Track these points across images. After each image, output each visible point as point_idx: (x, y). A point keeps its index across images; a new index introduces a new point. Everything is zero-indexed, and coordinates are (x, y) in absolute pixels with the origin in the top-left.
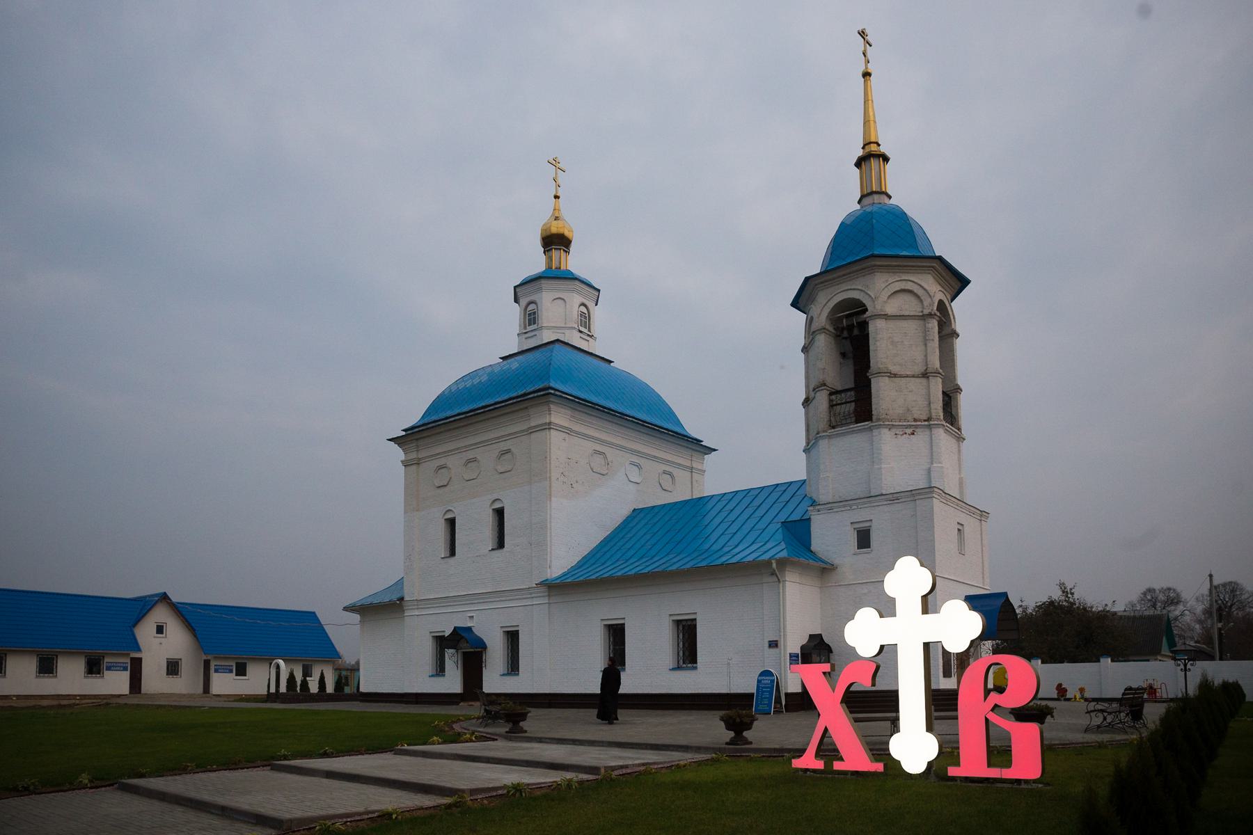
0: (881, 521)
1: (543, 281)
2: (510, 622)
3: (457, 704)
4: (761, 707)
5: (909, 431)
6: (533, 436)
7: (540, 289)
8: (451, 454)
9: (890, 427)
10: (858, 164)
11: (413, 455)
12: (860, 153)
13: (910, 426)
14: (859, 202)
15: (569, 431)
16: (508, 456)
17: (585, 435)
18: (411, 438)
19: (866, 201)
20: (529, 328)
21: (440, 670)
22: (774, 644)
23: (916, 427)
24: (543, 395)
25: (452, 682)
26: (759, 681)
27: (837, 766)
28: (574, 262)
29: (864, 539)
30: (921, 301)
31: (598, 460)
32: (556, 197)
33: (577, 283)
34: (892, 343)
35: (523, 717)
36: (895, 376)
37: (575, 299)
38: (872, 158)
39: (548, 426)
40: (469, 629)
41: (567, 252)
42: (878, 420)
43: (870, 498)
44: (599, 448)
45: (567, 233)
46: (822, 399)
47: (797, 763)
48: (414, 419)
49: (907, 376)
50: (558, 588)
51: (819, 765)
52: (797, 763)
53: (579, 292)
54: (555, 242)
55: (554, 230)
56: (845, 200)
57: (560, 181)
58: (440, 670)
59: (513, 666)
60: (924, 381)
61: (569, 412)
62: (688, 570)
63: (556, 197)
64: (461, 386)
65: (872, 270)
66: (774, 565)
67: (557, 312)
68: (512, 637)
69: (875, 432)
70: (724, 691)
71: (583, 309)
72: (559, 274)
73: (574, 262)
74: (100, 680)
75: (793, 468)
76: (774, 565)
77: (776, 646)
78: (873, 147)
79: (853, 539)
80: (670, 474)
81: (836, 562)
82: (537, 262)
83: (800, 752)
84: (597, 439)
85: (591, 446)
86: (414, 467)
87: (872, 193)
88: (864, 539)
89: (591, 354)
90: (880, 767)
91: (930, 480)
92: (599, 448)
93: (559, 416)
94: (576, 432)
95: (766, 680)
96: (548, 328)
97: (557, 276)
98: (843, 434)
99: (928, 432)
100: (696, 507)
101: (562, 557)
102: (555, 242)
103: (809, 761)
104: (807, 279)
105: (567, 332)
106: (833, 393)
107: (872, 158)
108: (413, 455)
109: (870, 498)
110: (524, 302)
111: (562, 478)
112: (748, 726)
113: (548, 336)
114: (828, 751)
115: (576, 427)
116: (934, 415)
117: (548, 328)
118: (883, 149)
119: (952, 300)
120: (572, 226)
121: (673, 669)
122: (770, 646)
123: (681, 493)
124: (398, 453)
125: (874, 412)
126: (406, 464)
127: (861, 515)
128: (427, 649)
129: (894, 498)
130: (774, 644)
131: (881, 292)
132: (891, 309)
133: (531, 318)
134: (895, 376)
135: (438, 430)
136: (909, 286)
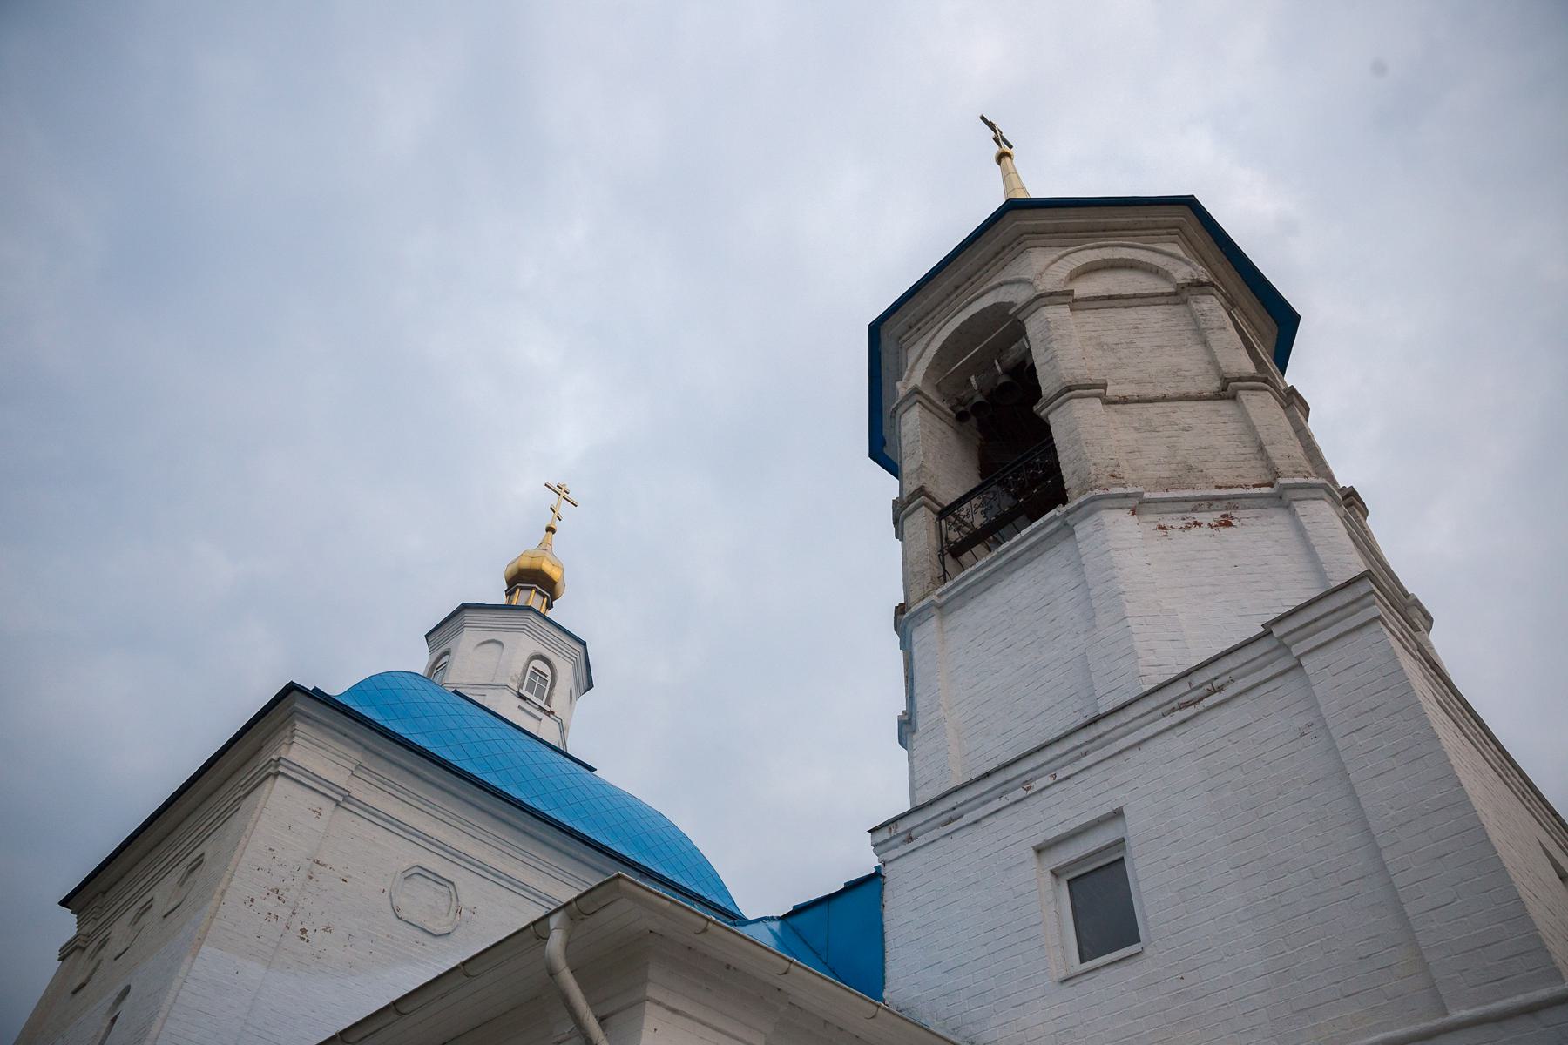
13: (1211, 501)
32: (550, 530)
34: (1100, 345)
46: (922, 522)
49: (1164, 399)
53: (532, 633)
60: (1225, 407)
61: (357, 756)
69: (1083, 529)
79: (1053, 914)
85: (410, 854)
89: (541, 741)
99: (1280, 517)
104: (875, 329)
106: (944, 513)
111: (271, 904)
116: (1282, 465)
119: (1282, 365)
120: (562, 562)
125: (1066, 471)
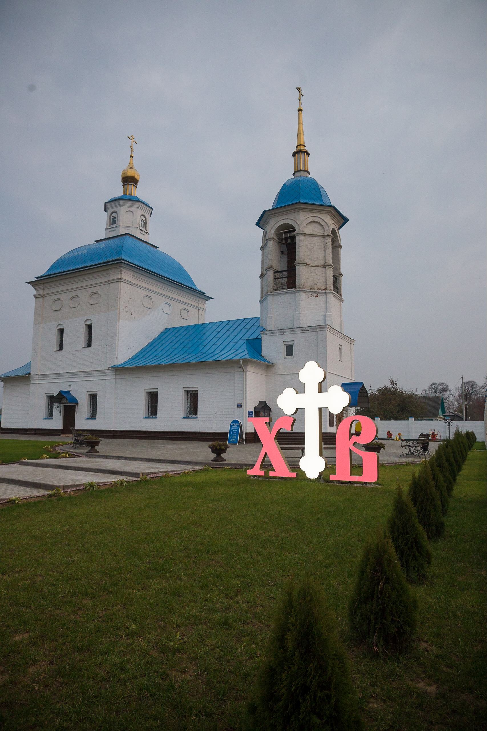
0: (299, 341)
1: (121, 201)
2: (93, 389)
3: (59, 435)
4: (231, 440)
5: (315, 295)
6: (111, 285)
7: (119, 205)
8: (82, 289)
9: (305, 292)
10: (294, 155)
11: (41, 292)
12: (295, 149)
14: (293, 175)
15: (132, 284)
16: (77, 299)
17: (140, 286)
18: (40, 282)
19: (298, 174)
20: (112, 226)
21: (50, 415)
22: (240, 406)
23: (319, 293)
24: (118, 263)
25: (57, 422)
26: (231, 426)
27: (271, 474)
28: (140, 192)
29: (290, 350)
30: (323, 228)
31: (146, 301)
32: (131, 157)
33: (140, 203)
35: (97, 443)
36: (309, 265)
37: (138, 212)
38: (300, 153)
39: (120, 280)
40: (68, 392)
41: (136, 187)
42: (299, 288)
43: (294, 329)
44: (147, 293)
45: (136, 176)
47: (250, 472)
48: (43, 271)
50: (120, 370)
51: (262, 473)
52: (250, 472)
54: (129, 180)
55: (129, 174)
56: (285, 173)
57: (133, 148)
58: (50, 415)
59: (93, 414)
60: (323, 269)
62: (194, 363)
63: (131, 157)
64: (71, 255)
65: (298, 210)
66: (241, 362)
67: (128, 219)
68: (93, 397)
69: (297, 294)
70: (212, 431)
71: (143, 218)
72: (130, 198)
73: (140, 192)
74: (94, 421)
75: (253, 310)
76: (241, 362)
77: (241, 406)
78: (302, 147)
80: (187, 310)
81: (275, 362)
82: (119, 191)
83: (251, 466)
84: (148, 289)
85: (142, 293)
86: (41, 299)
87: (300, 170)
88: (290, 350)
90: (294, 475)
91: (325, 322)
92: (147, 293)
93: (126, 275)
94: (135, 284)
95: (235, 425)
96: (123, 227)
97: (130, 199)
98: (281, 294)
100: (199, 329)
101: (123, 354)
102: (129, 180)
103: (257, 471)
105: (133, 230)
107: (300, 153)
108: (41, 292)
109: (294, 329)
110: (110, 211)
112: (224, 451)
113: (122, 231)
114: (267, 466)
115: (135, 282)
117: (123, 227)
118: (307, 149)
121: (184, 418)
122: (238, 407)
123: (192, 321)
124: (32, 290)
126: (36, 297)
127: (288, 337)
128: (43, 403)
129: (306, 329)
130: (240, 406)
131: (302, 221)
132: (308, 230)
133: (113, 221)
134: (309, 265)
135: (67, 277)
136: (317, 220)
